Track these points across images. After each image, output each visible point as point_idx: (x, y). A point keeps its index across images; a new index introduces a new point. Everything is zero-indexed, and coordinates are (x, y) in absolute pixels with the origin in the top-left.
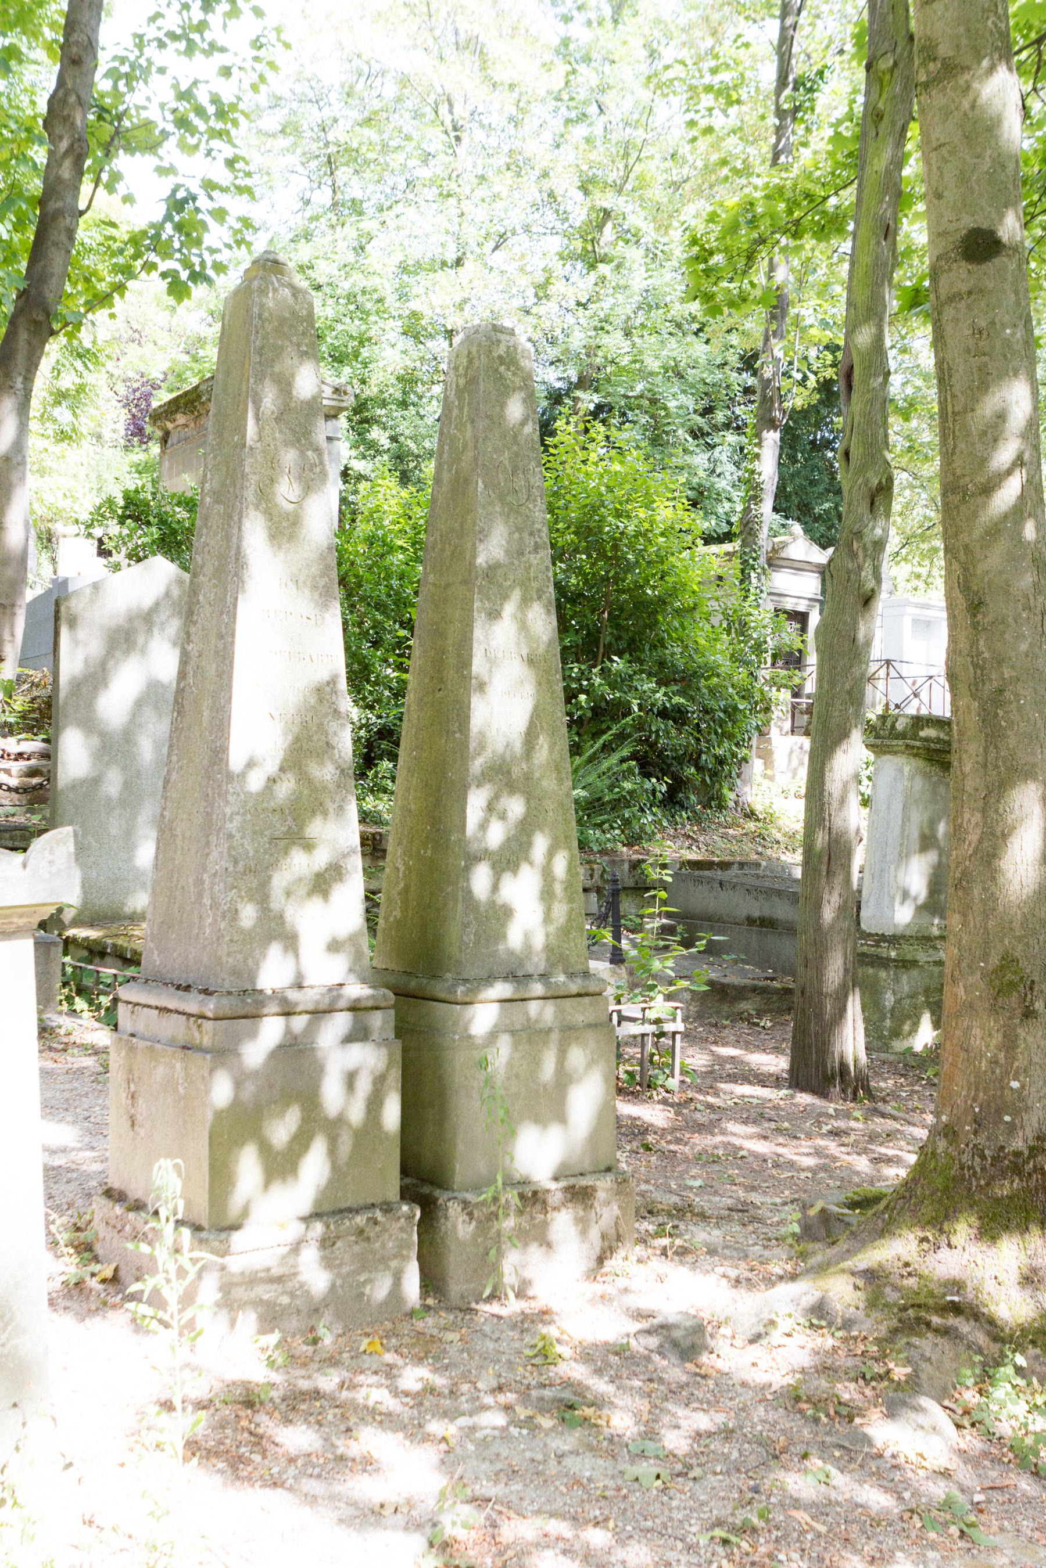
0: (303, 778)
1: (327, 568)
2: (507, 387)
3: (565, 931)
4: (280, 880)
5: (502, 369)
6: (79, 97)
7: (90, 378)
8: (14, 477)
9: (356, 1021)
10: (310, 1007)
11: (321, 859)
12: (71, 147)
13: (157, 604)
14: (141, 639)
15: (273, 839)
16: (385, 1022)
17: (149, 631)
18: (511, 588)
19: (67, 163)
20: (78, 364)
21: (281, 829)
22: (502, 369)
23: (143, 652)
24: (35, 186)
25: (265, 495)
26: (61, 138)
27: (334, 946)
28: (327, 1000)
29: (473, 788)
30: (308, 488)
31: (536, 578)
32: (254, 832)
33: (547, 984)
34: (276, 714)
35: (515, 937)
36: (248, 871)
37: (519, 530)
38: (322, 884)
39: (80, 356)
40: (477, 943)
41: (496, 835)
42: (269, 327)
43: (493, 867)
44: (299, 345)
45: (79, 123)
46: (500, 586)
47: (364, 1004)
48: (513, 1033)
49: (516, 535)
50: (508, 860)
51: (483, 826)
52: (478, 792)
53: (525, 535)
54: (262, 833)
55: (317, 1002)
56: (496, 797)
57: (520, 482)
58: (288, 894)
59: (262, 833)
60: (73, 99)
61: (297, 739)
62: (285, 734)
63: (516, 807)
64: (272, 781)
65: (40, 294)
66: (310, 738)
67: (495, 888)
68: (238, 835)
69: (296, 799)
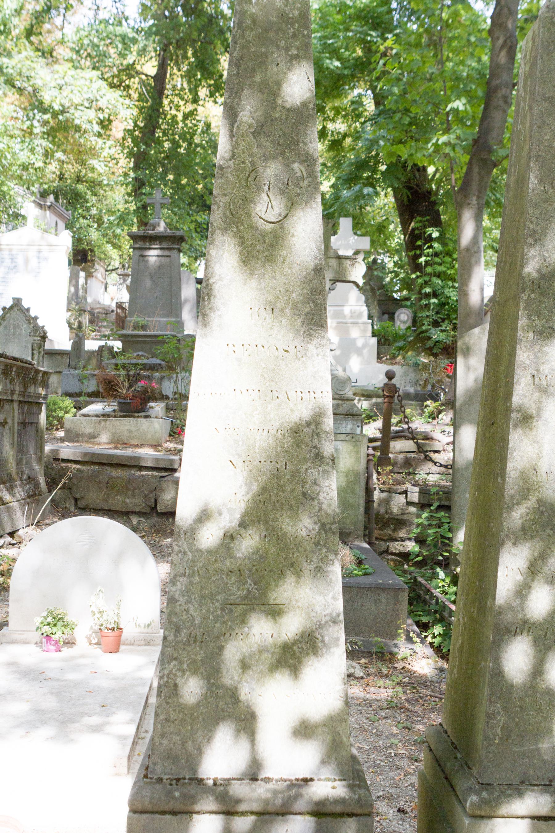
0: (274, 535)
4: (233, 652)
6: (509, 9)
8: (473, 260)
10: (255, 807)
11: (291, 626)
12: (505, 42)
15: (228, 606)
19: (503, 54)
21: (237, 592)
25: (238, 221)
26: (498, 38)
27: (304, 730)
28: (279, 801)
29: (508, 546)
30: (292, 204)
32: (203, 597)
34: (238, 462)
36: (193, 639)
38: (291, 657)
40: (506, 737)
42: (250, 35)
44: (287, 49)
47: (330, 809)
51: (522, 592)
52: (514, 550)
54: (212, 597)
55: (267, 802)
58: (245, 666)
59: (212, 597)
60: (506, 10)
61: (264, 490)
62: (249, 484)
64: (230, 537)
66: (281, 488)
67: (538, 671)
68: (182, 600)
69: (259, 559)
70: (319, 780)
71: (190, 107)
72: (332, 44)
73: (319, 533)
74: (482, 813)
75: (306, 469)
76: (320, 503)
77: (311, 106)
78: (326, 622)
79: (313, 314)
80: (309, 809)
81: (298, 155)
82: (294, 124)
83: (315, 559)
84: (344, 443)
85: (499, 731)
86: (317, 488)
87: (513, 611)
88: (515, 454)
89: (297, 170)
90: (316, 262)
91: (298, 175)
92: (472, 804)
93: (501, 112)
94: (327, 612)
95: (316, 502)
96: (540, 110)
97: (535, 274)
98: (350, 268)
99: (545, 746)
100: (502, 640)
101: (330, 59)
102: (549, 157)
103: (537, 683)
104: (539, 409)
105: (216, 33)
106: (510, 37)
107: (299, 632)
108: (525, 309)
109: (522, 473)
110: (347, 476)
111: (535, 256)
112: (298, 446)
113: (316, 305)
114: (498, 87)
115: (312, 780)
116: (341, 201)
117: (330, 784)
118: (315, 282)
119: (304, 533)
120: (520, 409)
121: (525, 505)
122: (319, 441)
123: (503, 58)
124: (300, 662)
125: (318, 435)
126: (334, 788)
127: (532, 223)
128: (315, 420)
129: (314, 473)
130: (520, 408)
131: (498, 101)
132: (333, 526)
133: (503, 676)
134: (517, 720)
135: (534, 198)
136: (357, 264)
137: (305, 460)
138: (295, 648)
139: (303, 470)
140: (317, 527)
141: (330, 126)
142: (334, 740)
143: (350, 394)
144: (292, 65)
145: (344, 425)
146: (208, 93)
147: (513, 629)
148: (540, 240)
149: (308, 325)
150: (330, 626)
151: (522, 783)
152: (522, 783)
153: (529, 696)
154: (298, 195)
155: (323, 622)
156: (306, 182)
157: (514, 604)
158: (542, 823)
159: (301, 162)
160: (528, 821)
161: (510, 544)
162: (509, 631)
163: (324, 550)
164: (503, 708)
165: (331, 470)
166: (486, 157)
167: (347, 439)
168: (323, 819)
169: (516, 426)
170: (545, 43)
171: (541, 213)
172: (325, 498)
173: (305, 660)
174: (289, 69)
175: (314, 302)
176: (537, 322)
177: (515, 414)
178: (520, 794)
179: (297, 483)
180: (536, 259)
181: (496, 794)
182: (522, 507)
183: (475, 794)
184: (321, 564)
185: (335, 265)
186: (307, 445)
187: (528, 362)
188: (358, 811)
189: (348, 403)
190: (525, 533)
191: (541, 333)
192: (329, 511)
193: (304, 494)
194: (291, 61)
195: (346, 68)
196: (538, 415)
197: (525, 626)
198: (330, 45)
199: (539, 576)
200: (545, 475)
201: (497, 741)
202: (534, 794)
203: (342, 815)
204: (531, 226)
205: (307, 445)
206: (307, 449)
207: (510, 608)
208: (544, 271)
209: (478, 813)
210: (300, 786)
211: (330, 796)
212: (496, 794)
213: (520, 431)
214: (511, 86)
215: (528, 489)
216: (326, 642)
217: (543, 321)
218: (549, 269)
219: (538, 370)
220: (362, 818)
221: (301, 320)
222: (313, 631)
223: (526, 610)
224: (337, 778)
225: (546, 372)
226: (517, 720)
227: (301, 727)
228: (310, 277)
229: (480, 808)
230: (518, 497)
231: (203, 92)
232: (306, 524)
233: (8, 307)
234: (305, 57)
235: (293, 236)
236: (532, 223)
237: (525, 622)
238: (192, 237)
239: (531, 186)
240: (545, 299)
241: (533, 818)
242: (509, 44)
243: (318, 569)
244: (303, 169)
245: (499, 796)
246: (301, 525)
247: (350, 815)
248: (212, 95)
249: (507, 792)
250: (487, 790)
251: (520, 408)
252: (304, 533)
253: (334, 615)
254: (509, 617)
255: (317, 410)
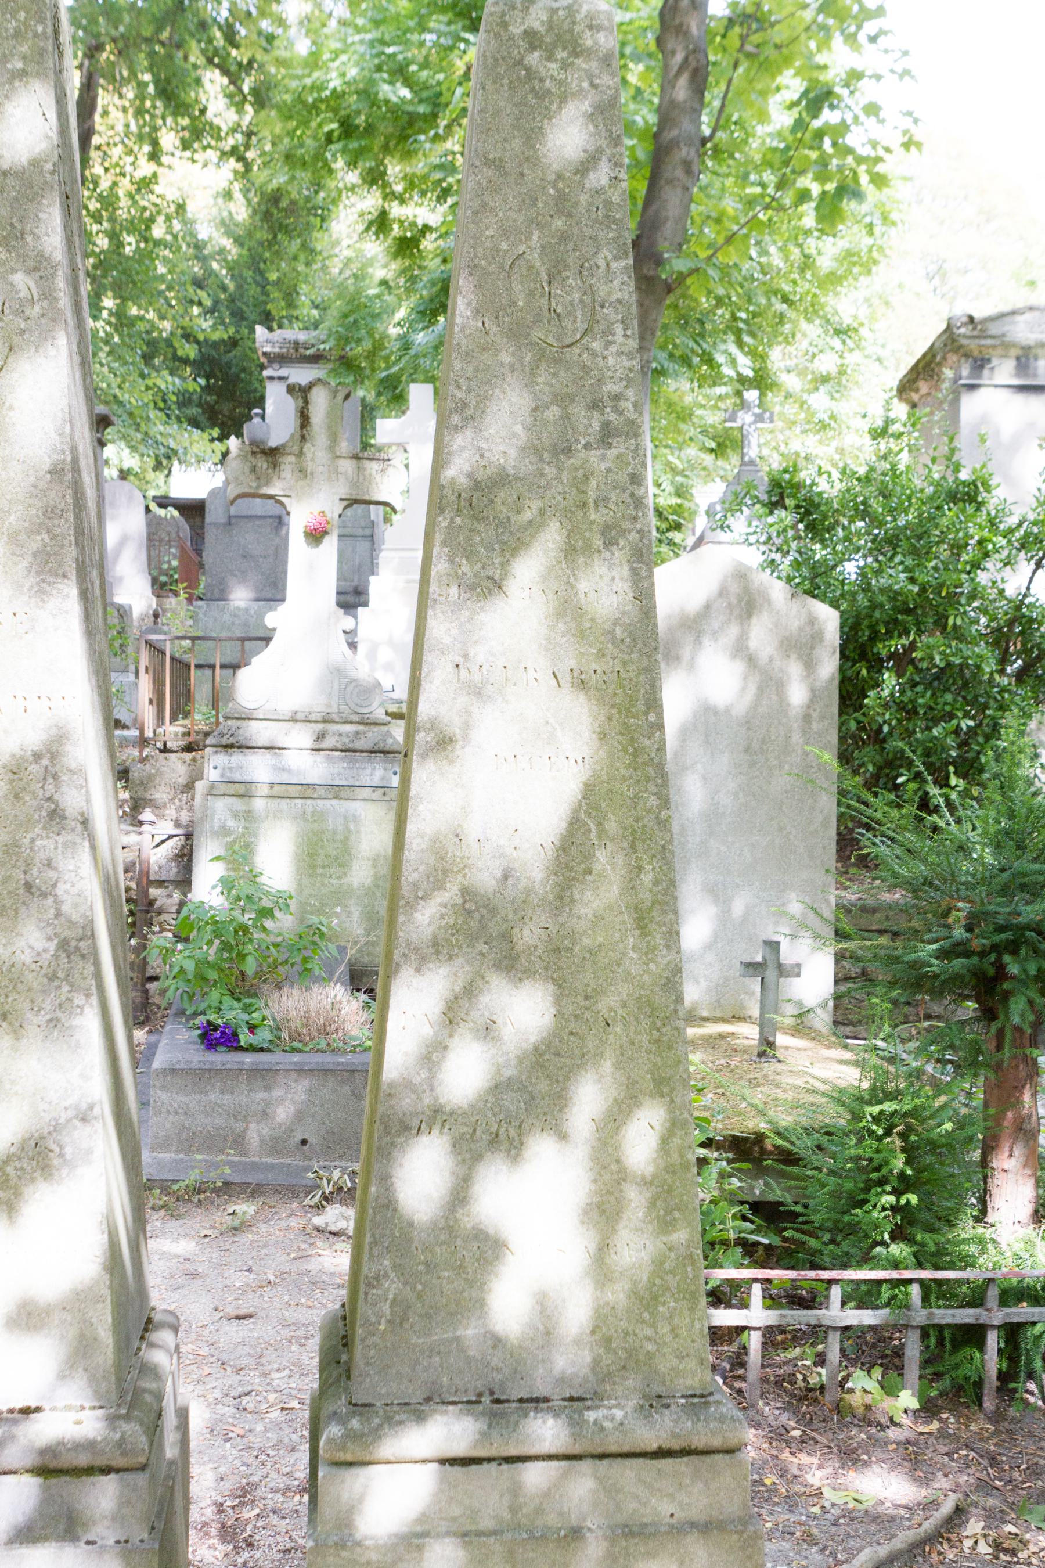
1: (50, 512)
2: (542, 95)
3: (647, 1299)
5: (534, 58)
7: (851, 359)
9: (47, 1499)
12: (686, 59)
13: (707, 607)
14: (686, 652)
16: (124, 1502)
17: (698, 642)
18: (535, 527)
19: (683, 81)
20: (836, 342)
22: (534, 58)
23: (691, 666)
24: (645, 117)
26: (673, 53)
31: (602, 501)
33: (576, 1424)
35: (508, 1306)
37: (561, 399)
39: (838, 332)
40: (398, 1322)
41: (466, 1075)
43: (457, 1145)
45: (694, 30)
46: (504, 523)
47: (66, 1461)
48: (466, 1536)
49: (553, 412)
50: (495, 1130)
51: (432, 1055)
52: (417, 981)
53: (579, 411)
56: (469, 992)
57: (570, 293)
63: (525, 1011)
65: (653, 244)
67: (460, 1194)
70: (53, 1409)
71: (146, 168)
72: (394, 55)
73: (56, 957)
74: (349, 1457)
75: (33, 841)
76: (58, 903)
77: (49, 166)
78: (69, 1121)
79: (49, 554)
80: (29, 1461)
81: (23, 257)
82: (16, 199)
83: (47, 1005)
84: (369, 805)
85: (386, 1308)
86: (52, 874)
87: (414, 1092)
88: (421, 807)
89: (21, 286)
90: (55, 457)
91: (22, 295)
92: (330, 1441)
93: (679, 190)
94: (70, 1102)
95: (50, 900)
96: (479, 183)
97: (463, 480)
98: (378, 478)
99: (470, 1332)
100: (393, 1144)
101: (391, 83)
102: (492, 268)
103: (456, 1221)
104: (467, 726)
105: (193, 28)
106: (694, 51)
107: (17, 1139)
108: (444, 543)
109: (435, 840)
110: (375, 866)
111: (463, 449)
112: (17, 797)
113: (54, 537)
114: (675, 143)
115: (38, 1409)
116: (412, 352)
117: (73, 1416)
118: (52, 494)
119: (27, 957)
120: (433, 725)
121: (439, 900)
122: (57, 787)
123: (681, 91)
124: (18, 1194)
125: (55, 776)
126: (78, 1423)
127: (459, 387)
128: (48, 750)
129: (47, 845)
130: (433, 724)
131: (673, 170)
132: (82, 944)
133: (395, 1210)
134: (419, 1287)
135: (464, 342)
136: (390, 470)
137: (28, 823)
138: (9, 1169)
139: (26, 841)
140: (52, 946)
141: (396, 210)
142: (82, 1336)
143: (380, 714)
144: (13, 89)
145: (368, 771)
146: (178, 143)
147: (415, 1123)
148: (473, 418)
149: (38, 573)
150: (75, 1128)
151: (428, 1399)
152: (428, 1399)
153: (443, 1243)
154: (22, 332)
155: (62, 1121)
156: (37, 309)
157: (417, 1080)
158: (457, 1470)
159: (30, 271)
160: (435, 1465)
161: (411, 971)
162: (407, 1128)
163: (66, 988)
164: (395, 1267)
165: (78, 840)
166: (651, 273)
167: (375, 796)
168: (53, 1481)
169: (424, 756)
170: (490, 61)
171: (476, 370)
172: (67, 892)
173: (27, 1191)
174: (7, 97)
175: (49, 532)
176: (466, 568)
177: (422, 734)
178: (420, 1417)
179: (14, 866)
180: (466, 454)
181: (377, 1421)
182: (432, 902)
183: (338, 1423)
184: (59, 1014)
185: (350, 471)
186: (35, 796)
187: (447, 640)
188: (119, 1462)
189: (376, 729)
190: (438, 949)
191: (472, 588)
192: (75, 917)
193: (28, 886)
194: (11, 81)
195: (421, 101)
196: (465, 736)
197: (437, 1117)
198: (389, 56)
199: (463, 1029)
200: (475, 846)
201: (382, 1327)
202: (445, 1419)
203: (90, 1471)
204: (458, 394)
205: (35, 796)
206: (34, 803)
207: (409, 1085)
208: (480, 475)
209: (341, 1456)
210: (15, 1422)
211: (68, 1437)
212: (377, 1421)
213: (430, 765)
214: (698, 143)
215: (444, 872)
216: (68, 1157)
217: (477, 567)
218: (489, 472)
219: (465, 656)
220: (126, 1475)
221: (25, 564)
222: (43, 1138)
223: (438, 1090)
224: (87, 1405)
225: (481, 659)
226: (419, 1287)
227: (19, 1314)
228: (42, 485)
229: (344, 1448)
230: (425, 885)
231: (168, 139)
232: (32, 942)
233: (372, 578)
234: (38, 75)
235: (11, 408)
236: (459, 387)
237: (437, 1110)
238: (148, 418)
239: (458, 320)
240: (481, 528)
241: (443, 1462)
242: (694, 64)
243: (54, 1023)
244: (32, 285)
245: (381, 1426)
246: (23, 943)
247: (106, 1470)
248: (186, 145)
249: (397, 1418)
250: (361, 1414)
251: (433, 724)
252: (27, 957)
253: (84, 1106)
254: (406, 1102)
255: (54, 731)
